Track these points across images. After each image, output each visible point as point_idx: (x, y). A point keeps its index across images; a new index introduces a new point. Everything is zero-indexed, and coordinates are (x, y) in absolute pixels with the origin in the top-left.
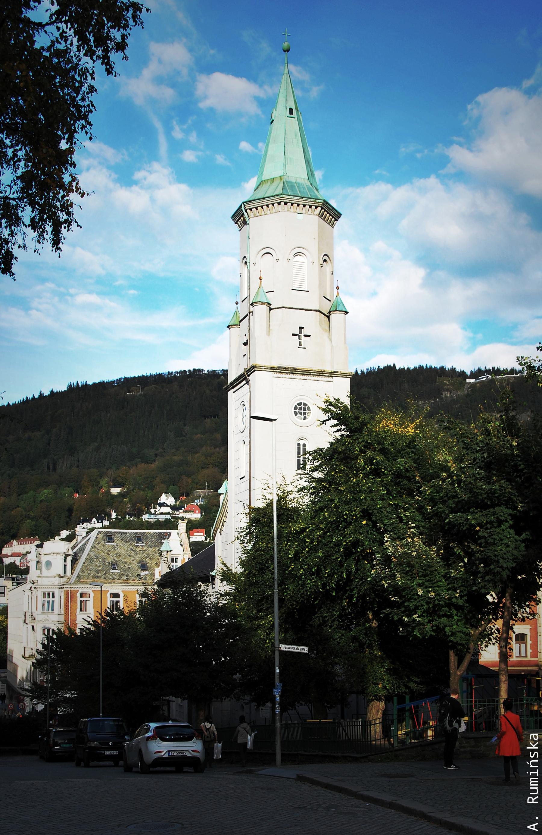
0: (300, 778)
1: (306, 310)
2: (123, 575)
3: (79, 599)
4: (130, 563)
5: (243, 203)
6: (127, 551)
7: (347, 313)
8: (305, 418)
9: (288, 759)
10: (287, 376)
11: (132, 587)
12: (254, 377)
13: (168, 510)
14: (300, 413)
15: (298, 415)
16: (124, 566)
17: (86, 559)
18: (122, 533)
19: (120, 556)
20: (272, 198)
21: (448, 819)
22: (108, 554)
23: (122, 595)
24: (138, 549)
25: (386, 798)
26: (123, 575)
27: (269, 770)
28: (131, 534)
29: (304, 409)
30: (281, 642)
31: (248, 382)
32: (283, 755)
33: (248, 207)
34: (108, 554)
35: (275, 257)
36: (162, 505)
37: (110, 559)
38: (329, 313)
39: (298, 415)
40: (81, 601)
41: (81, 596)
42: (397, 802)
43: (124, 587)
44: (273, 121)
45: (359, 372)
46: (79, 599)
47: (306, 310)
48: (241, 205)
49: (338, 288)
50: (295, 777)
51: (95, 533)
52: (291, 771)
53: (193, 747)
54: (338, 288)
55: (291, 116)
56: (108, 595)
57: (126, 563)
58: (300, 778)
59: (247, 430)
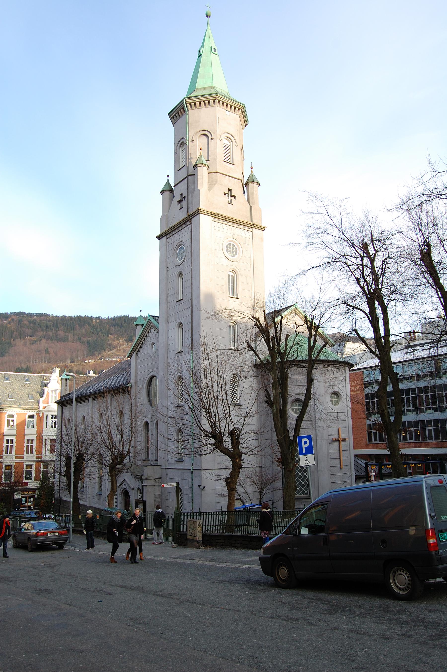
1: (233, 177)
2: (16, 402)
4: (22, 395)
5: (185, 98)
6: (19, 387)
8: (234, 256)
11: (24, 410)
14: (230, 252)
15: (229, 252)
16: (18, 396)
18: (15, 375)
19: (14, 390)
20: (209, 96)
22: (6, 388)
23: (16, 416)
24: (26, 386)
26: (16, 402)
29: (233, 249)
31: (191, 223)
33: (189, 101)
34: (6, 388)
37: (8, 391)
39: (229, 252)
43: (17, 410)
44: (201, 54)
45: (110, 318)
47: (233, 177)
48: (183, 100)
55: (215, 53)
56: (6, 416)
57: (18, 394)
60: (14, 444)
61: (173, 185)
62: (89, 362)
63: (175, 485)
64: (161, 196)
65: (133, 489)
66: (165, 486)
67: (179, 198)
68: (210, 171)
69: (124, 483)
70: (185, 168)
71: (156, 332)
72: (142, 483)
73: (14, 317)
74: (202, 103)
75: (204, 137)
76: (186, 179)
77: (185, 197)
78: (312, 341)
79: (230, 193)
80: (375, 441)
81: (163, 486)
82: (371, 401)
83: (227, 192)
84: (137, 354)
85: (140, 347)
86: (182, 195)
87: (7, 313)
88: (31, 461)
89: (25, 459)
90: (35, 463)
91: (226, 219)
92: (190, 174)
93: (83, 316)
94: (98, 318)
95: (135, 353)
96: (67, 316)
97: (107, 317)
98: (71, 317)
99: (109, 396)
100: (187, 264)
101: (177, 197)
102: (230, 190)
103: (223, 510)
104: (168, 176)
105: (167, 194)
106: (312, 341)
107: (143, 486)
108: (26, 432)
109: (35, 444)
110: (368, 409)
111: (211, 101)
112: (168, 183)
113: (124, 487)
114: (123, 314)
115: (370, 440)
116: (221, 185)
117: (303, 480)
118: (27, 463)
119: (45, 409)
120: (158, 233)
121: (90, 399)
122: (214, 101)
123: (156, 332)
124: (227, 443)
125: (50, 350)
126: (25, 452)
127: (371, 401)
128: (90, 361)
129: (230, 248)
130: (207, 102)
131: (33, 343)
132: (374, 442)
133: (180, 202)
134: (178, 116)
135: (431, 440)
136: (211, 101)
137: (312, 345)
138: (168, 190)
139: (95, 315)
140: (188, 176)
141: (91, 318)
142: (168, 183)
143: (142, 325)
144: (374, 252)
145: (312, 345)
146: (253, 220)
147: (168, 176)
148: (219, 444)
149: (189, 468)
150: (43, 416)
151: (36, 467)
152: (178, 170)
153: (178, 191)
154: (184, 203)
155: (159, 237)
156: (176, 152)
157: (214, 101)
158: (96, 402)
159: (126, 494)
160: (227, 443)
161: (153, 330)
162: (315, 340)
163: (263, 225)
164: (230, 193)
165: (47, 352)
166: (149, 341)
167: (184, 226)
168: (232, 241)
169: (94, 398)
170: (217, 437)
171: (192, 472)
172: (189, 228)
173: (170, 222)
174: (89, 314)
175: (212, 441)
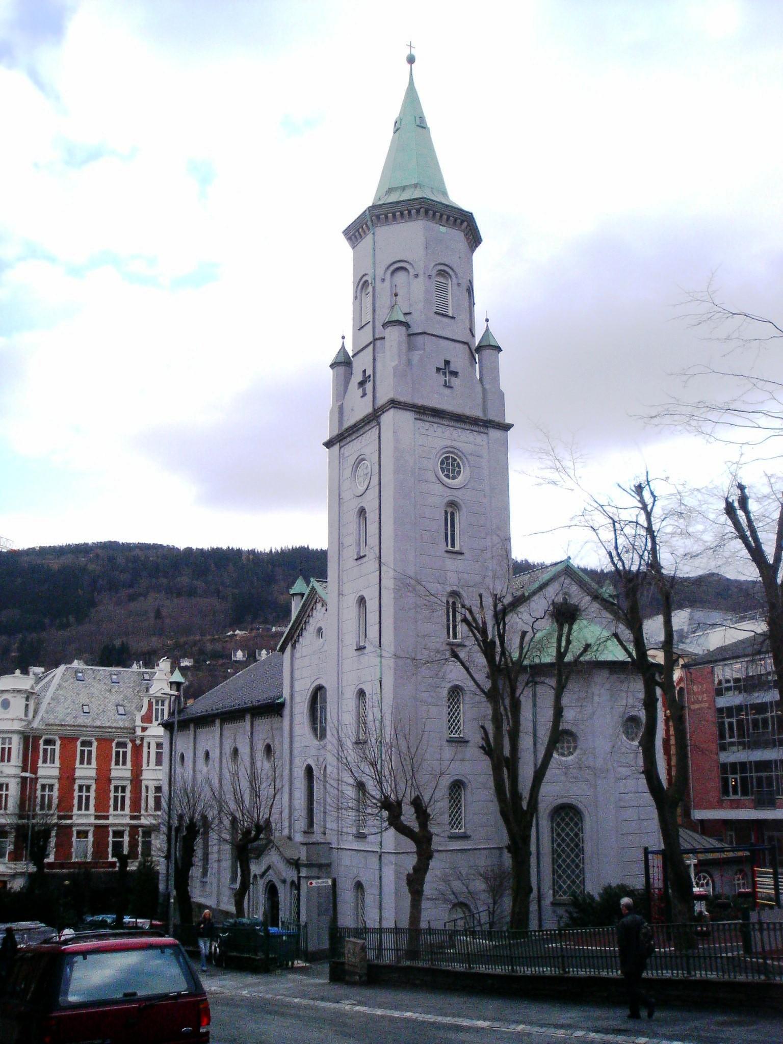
12: (388, 418)
17: (52, 699)
22: (78, 694)
29: (453, 465)
31: (379, 424)
45: (273, 551)
46: (42, 747)
60: (92, 794)
61: (351, 354)
62: (236, 635)
63: (330, 882)
64: (330, 371)
65: (284, 881)
66: (314, 884)
67: (360, 378)
68: (411, 331)
69: (270, 872)
70: (370, 326)
71: (324, 608)
72: (299, 872)
73: (99, 551)
77: (369, 376)
78: (563, 643)
79: (447, 369)
81: (311, 883)
82: (727, 721)
84: (294, 647)
85: (299, 636)
86: (364, 371)
87: (86, 545)
88: (123, 825)
89: (111, 821)
90: (128, 829)
92: (377, 337)
93: (225, 548)
94: (252, 552)
95: (289, 646)
96: (194, 548)
97: (267, 551)
98: (201, 551)
99: (248, 718)
100: (373, 493)
101: (357, 377)
103: (400, 926)
104: (343, 337)
105: (341, 369)
106: (563, 643)
107: (299, 878)
109: (128, 794)
110: (722, 736)
112: (343, 349)
113: (269, 878)
114: (298, 544)
115: (725, 792)
117: (573, 872)
118: (115, 828)
119: (146, 733)
120: (327, 438)
121: (218, 722)
122: (418, 211)
123: (324, 608)
124: (409, 816)
125: (164, 612)
126: (111, 809)
127: (727, 721)
128: (237, 632)
129: (448, 464)
131: (132, 598)
132: (732, 797)
133: (362, 384)
134: (358, 237)
137: (562, 650)
138: (343, 363)
139: (246, 546)
140: (375, 340)
141: (239, 552)
142: (343, 349)
143: (302, 595)
144: (652, 500)
145: (562, 650)
147: (343, 337)
148: (395, 821)
149: (374, 850)
150: (142, 745)
151: (130, 835)
152: (360, 327)
153: (362, 364)
154: (369, 386)
155: (329, 444)
156: (356, 298)
157: (418, 211)
158: (227, 726)
159: (272, 891)
160: (409, 816)
161: (319, 605)
162: (569, 642)
163: (508, 420)
164: (447, 369)
165: (158, 615)
166: (311, 629)
167: (367, 428)
168: (448, 452)
169: (223, 722)
170: (392, 808)
171: (380, 856)
172: (375, 431)
173: (345, 418)
174: (235, 545)
175: (385, 814)
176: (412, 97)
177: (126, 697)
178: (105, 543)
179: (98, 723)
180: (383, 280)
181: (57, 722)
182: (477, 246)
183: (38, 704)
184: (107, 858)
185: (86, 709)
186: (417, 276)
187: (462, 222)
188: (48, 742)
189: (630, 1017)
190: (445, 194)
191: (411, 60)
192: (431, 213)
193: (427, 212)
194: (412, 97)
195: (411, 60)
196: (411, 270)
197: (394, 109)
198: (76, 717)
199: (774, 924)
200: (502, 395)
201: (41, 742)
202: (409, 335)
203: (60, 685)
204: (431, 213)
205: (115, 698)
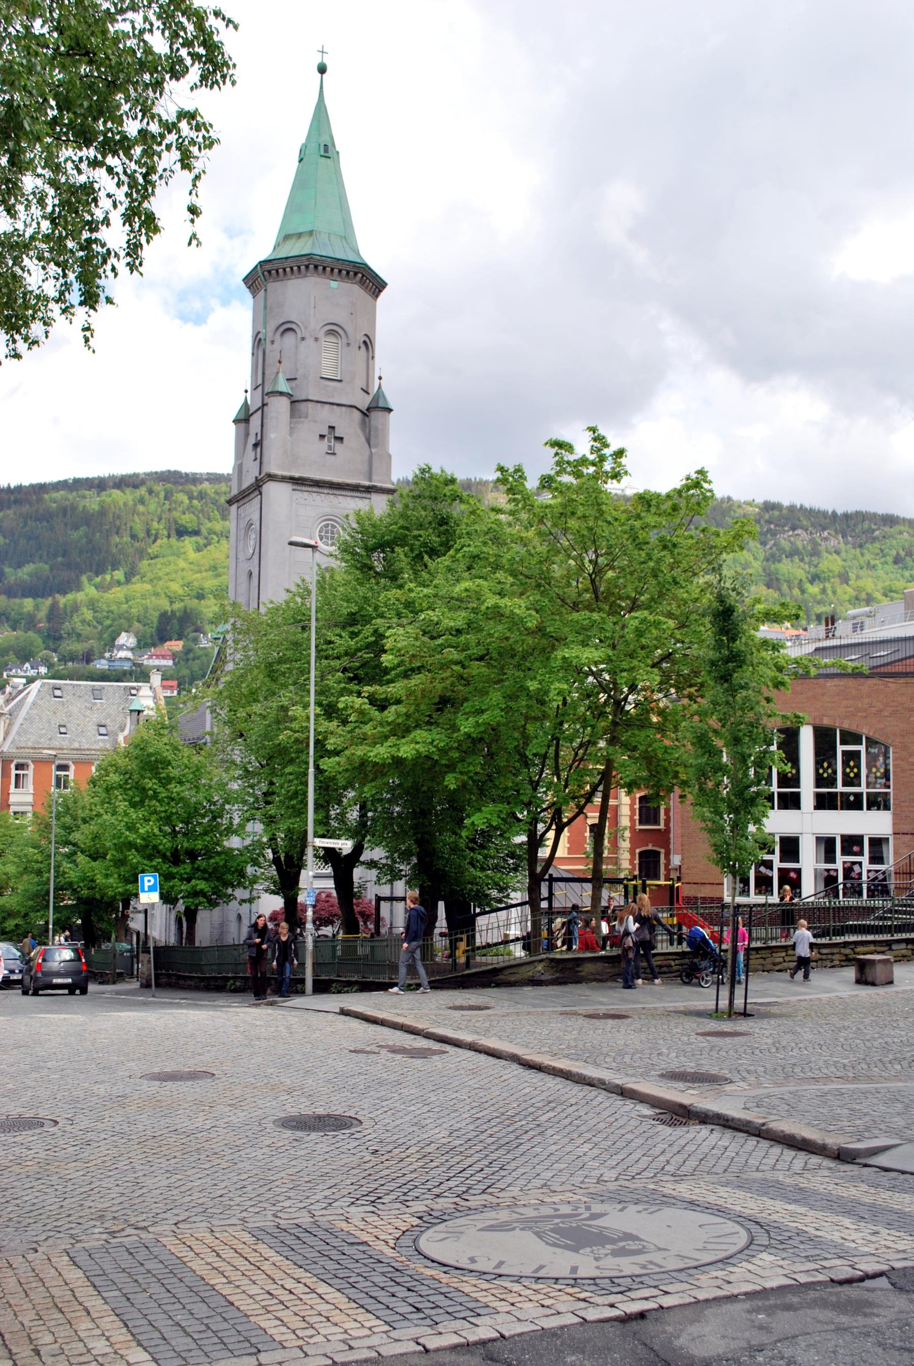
0: (344, 1012)
1: (338, 405)
3: (14, 772)
7: (390, 410)
9: (321, 987)
10: (310, 489)
12: (271, 488)
13: (129, 654)
17: (25, 719)
18: (74, 686)
21: (551, 1063)
25: (467, 1037)
27: (297, 1001)
28: (86, 686)
30: (316, 835)
31: (261, 494)
32: (315, 982)
35: (299, 336)
36: (121, 648)
38: (368, 409)
40: (17, 776)
41: (18, 767)
42: (481, 1042)
46: (14, 772)
47: (338, 405)
49: (380, 378)
50: (338, 1010)
51: (38, 683)
52: (332, 1002)
53: (339, 953)
54: (380, 378)
58: (344, 1012)
59: (256, 557)
64: (233, 426)
68: (293, 399)
74: (288, 270)
75: (290, 334)
76: (260, 412)
79: (333, 436)
80: (759, 892)
83: (325, 431)
91: (318, 484)
102: (332, 428)
105: (243, 425)
108: (13, 799)
111: (303, 268)
116: (315, 422)
122: (307, 267)
129: (327, 532)
130: (295, 268)
135: (853, 902)
136: (303, 268)
146: (374, 477)
157: (307, 267)
164: (333, 436)
176: (321, 114)
177: (109, 715)
178: (162, 473)
179: (76, 745)
180: (273, 342)
181: (30, 744)
182: (380, 291)
183: (10, 724)
184: (842, 743)
185: (63, 730)
186: (303, 339)
187: (356, 274)
188: (19, 767)
189: (859, 982)
190: (347, 235)
191: (322, 70)
192: (320, 268)
193: (316, 267)
194: (321, 114)
195: (322, 70)
196: (298, 330)
197: (298, 133)
198: (50, 739)
199: (696, 898)
200: (390, 456)
201: (13, 766)
202: (292, 402)
203: (34, 704)
204: (320, 268)
205: (96, 718)
